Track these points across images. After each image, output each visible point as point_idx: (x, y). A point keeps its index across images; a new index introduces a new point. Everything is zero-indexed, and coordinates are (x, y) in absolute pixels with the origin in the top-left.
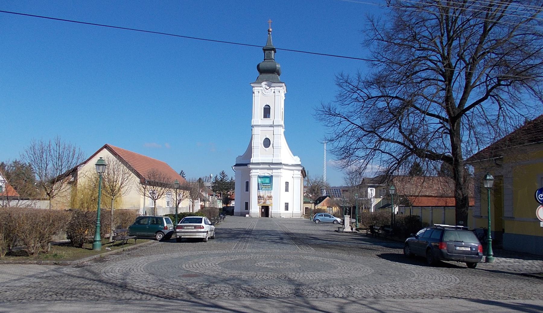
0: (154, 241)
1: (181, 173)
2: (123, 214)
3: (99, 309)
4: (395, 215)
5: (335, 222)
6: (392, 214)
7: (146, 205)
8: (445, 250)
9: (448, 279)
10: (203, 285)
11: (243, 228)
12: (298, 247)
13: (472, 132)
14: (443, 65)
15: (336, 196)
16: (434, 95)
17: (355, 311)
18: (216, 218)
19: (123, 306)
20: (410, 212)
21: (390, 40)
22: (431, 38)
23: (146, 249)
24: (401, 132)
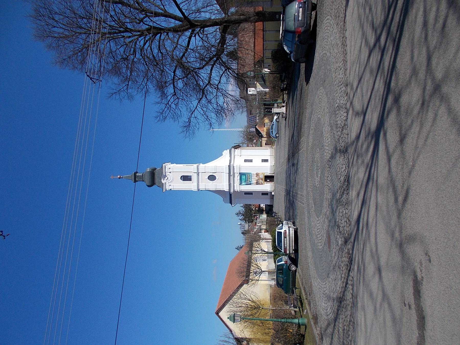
0: (297, 272)
1: (237, 249)
2: (275, 299)
3: (362, 322)
4: (271, 71)
5: (278, 120)
6: (270, 73)
7: (266, 279)
8: (302, 29)
9: (328, 26)
10: (338, 231)
11: (284, 197)
12: (301, 151)
13: (203, 10)
14: (147, 35)
15: (255, 120)
16: (173, 42)
17: (360, 102)
18: (276, 220)
19: (359, 300)
20: (269, 58)
21: (127, 79)
22: (125, 46)
23: (305, 280)
24: (202, 68)
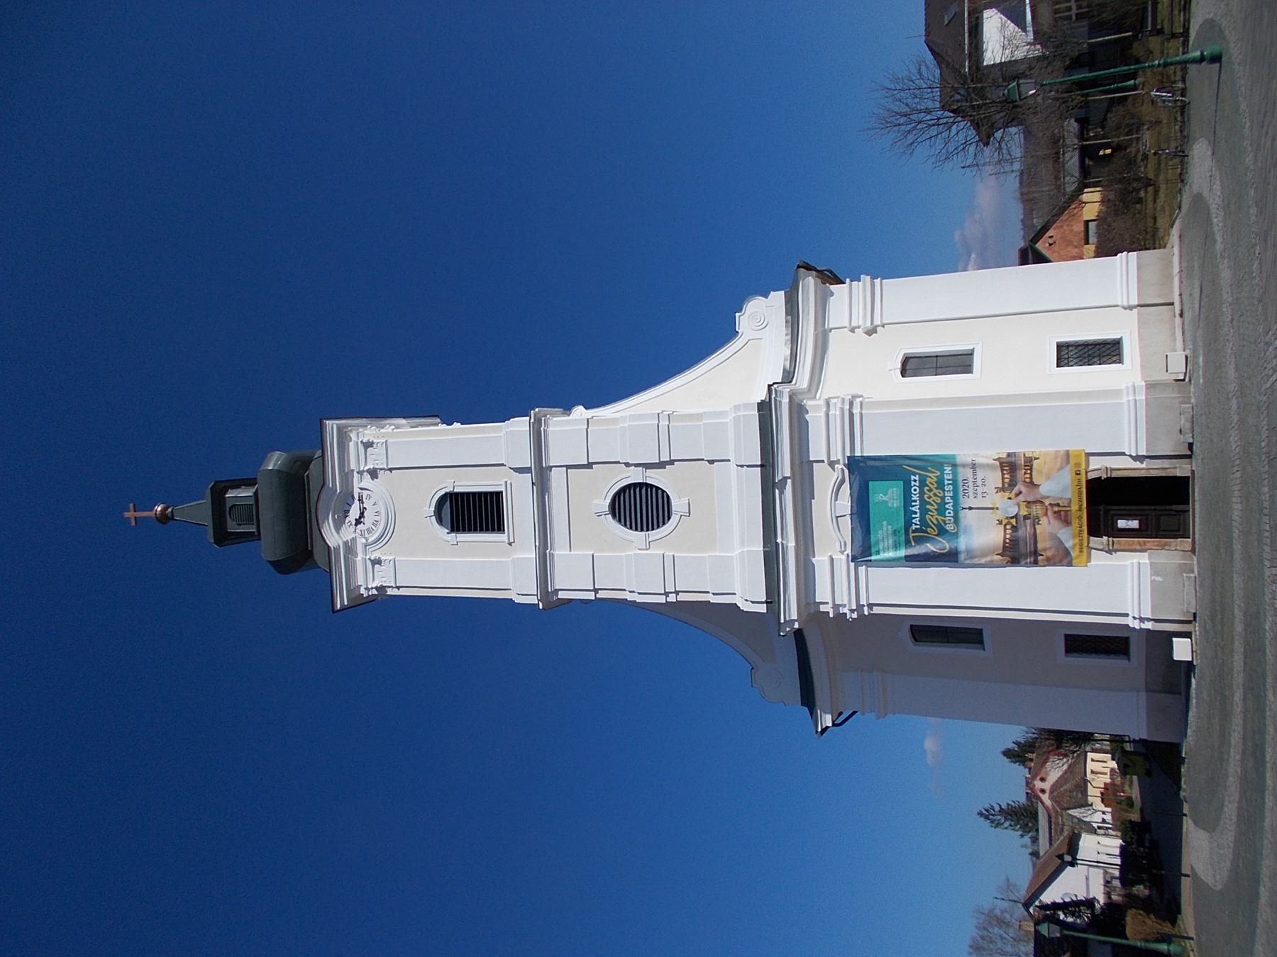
1: (987, 818)
